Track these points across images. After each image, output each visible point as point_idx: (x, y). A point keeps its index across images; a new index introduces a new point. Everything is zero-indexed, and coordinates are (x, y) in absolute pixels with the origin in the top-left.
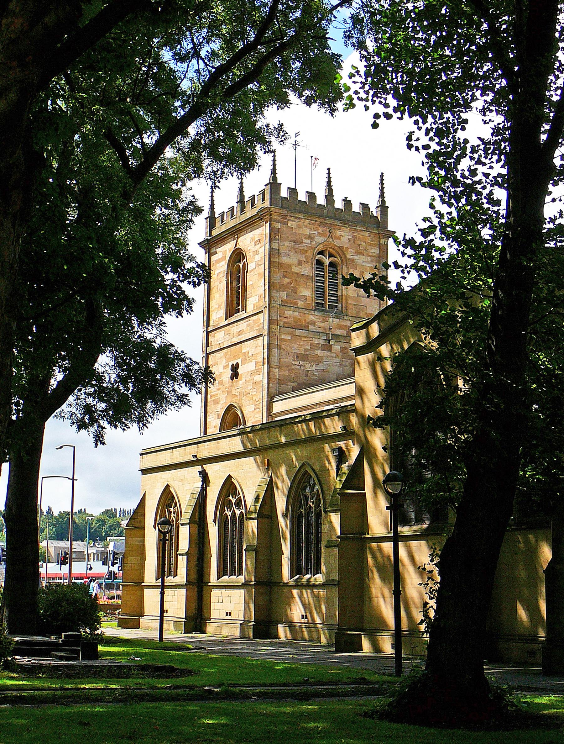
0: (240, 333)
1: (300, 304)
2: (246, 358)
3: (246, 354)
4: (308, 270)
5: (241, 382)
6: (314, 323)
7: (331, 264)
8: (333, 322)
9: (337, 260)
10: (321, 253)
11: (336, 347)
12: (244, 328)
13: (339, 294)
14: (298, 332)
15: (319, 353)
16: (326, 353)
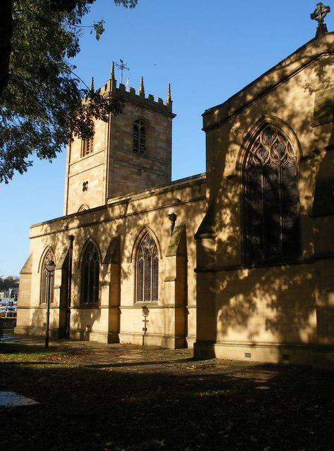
0: (89, 165)
1: (125, 148)
2: (92, 178)
3: (93, 175)
4: (130, 130)
5: (88, 193)
6: (132, 160)
7: (142, 129)
8: (142, 160)
9: (145, 126)
10: (137, 121)
11: (144, 174)
12: (91, 161)
13: (146, 145)
14: (124, 164)
15: (135, 176)
16: (138, 177)
